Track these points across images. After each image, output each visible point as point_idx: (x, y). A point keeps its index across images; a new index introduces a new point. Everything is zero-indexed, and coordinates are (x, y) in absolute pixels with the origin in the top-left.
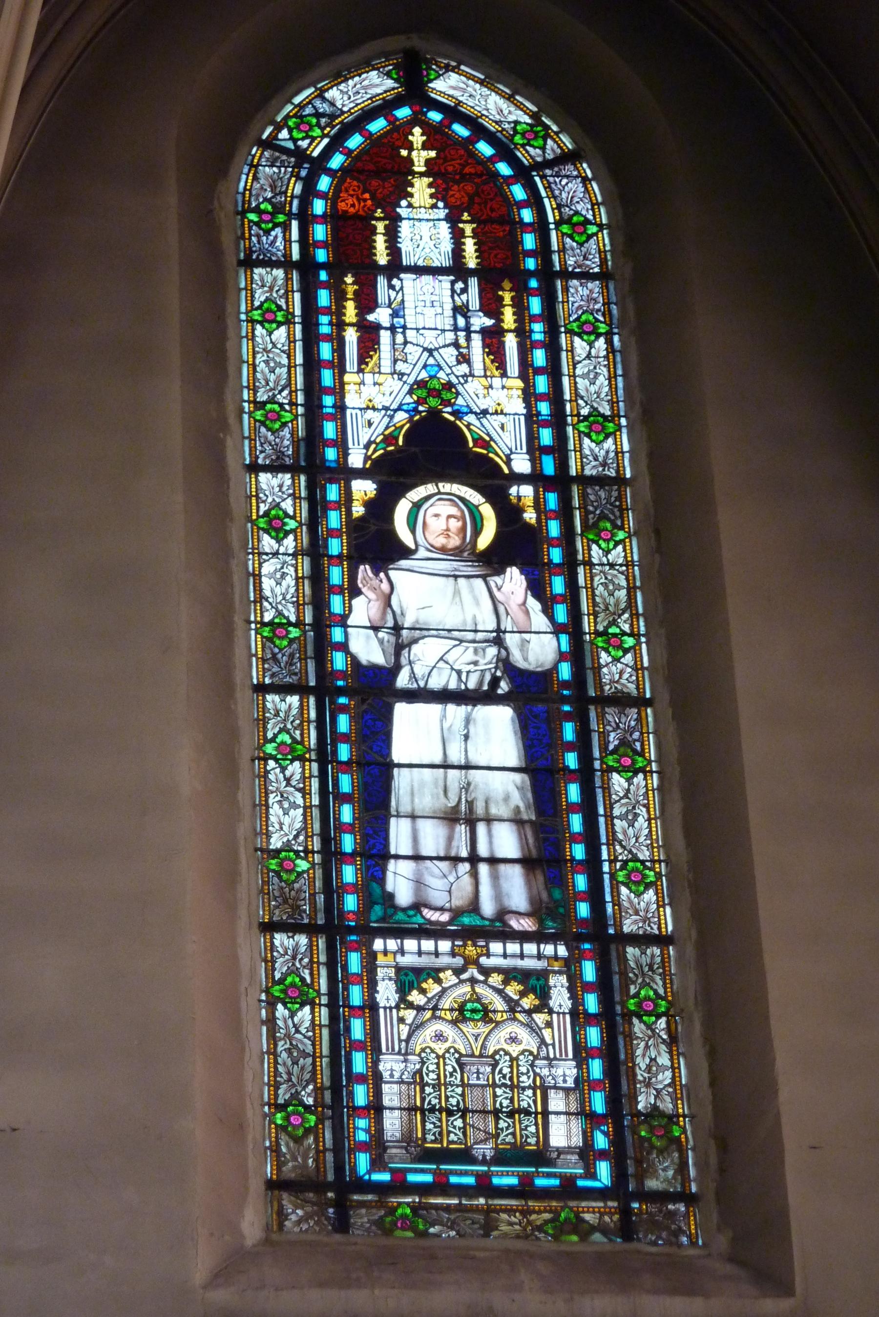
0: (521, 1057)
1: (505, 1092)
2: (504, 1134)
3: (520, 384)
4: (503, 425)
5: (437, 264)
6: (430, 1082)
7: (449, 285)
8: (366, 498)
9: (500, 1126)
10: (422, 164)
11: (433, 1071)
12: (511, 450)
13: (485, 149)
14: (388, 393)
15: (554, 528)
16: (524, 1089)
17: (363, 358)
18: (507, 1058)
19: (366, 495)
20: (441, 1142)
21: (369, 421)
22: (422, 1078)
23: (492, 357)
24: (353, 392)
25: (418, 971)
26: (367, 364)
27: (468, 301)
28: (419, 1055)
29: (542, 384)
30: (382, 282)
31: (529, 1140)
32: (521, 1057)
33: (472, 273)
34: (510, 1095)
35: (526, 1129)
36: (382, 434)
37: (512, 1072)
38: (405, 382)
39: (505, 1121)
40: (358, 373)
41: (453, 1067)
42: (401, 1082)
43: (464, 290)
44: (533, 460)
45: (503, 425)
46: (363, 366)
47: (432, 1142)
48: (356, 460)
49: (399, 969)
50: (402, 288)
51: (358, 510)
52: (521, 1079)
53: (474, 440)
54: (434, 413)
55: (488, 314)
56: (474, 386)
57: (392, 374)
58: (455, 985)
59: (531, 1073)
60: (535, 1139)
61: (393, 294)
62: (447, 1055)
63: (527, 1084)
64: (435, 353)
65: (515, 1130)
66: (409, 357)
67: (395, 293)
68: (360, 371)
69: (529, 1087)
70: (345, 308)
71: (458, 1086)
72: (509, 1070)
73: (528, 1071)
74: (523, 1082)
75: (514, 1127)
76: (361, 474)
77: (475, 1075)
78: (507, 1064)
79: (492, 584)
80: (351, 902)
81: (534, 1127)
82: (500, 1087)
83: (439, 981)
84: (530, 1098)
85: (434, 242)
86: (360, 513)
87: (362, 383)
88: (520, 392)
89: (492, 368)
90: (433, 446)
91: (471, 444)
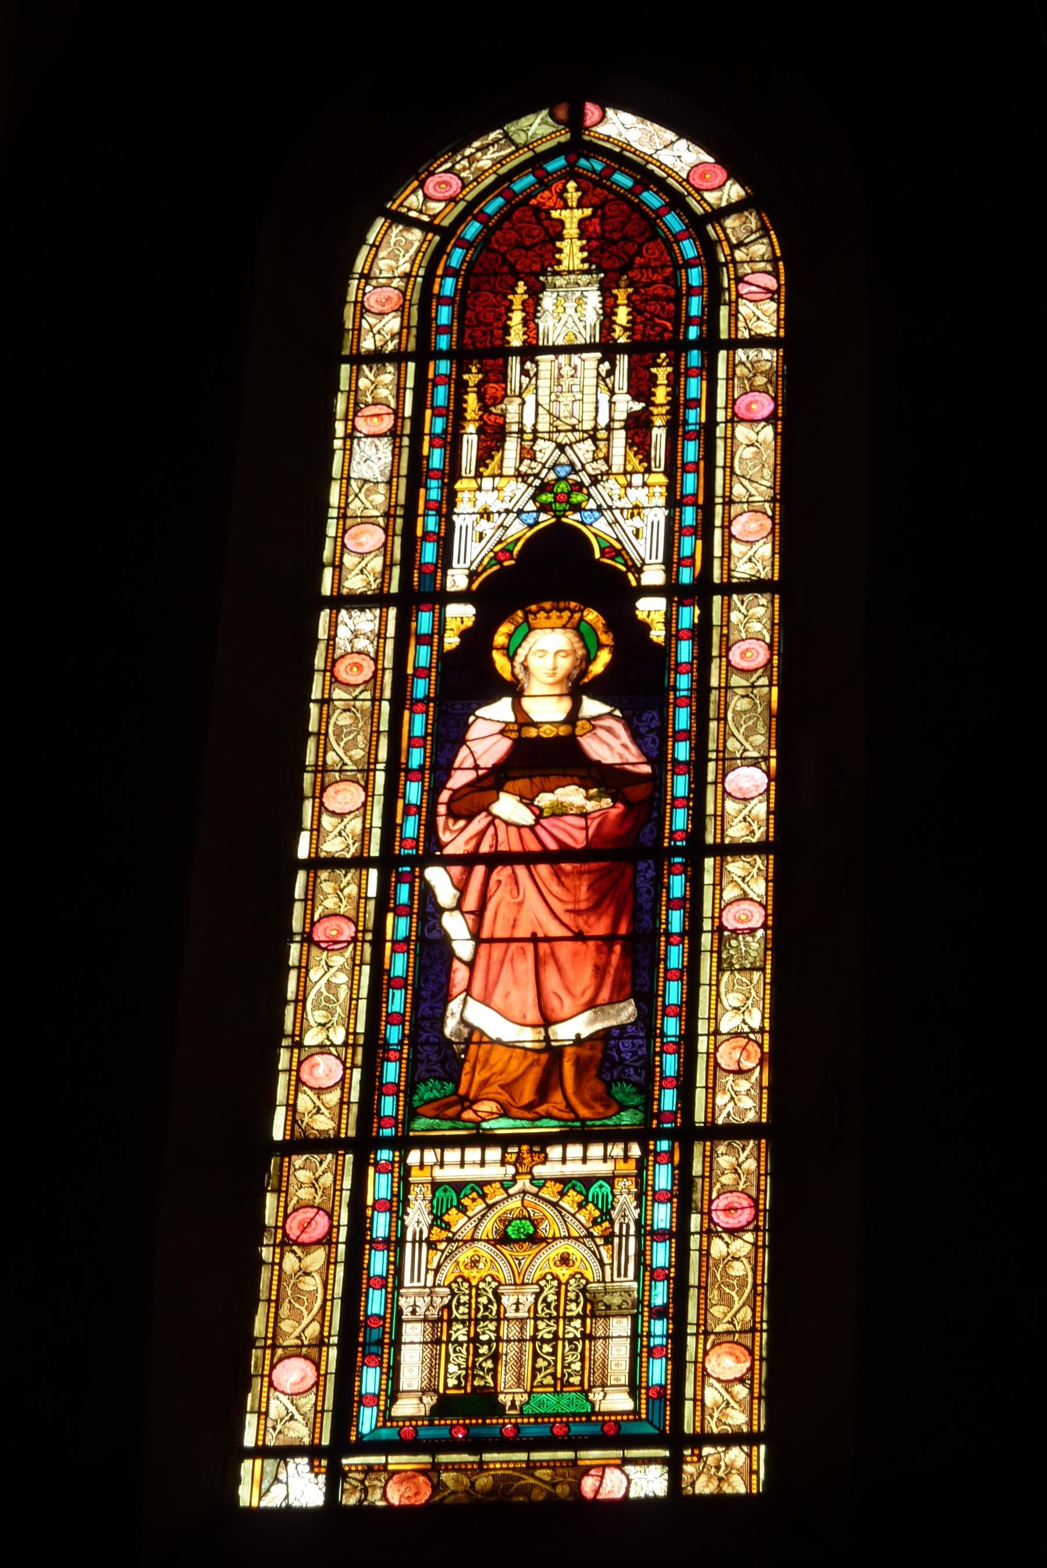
0: (572, 1281)
1: (548, 1325)
2: (543, 1374)
3: (663, 479)
4: (638, 530)
5: (581, 341)
6: (459, 1317)
7: (594, 364)
8: (462, 627)
9: (537, 1366)
10: (575, 225)
11: (464, 1304)
12: (643, 560)
13: (652, 199)
14: (507, 499)
15: (685, 651)
16: (571, 1319)
17: (484, 458)
18: (555, 1283)
19: (462, 622)
20: (465, 1388)
21: (481, 534)
22: (450, 1313)
23: (635, 449)
24: (466, 500)
25: (458, 1186)
26: (486, 466)
27: (613, 385)
28: (449, 1286)
29: (690, 483)
30: (515, 363)
31: (572, 1380)
32: (572, 1281)
33: (622, 349)
34: (554, 1329)
35: (569, 1367)
36: (492, 550)
37: (558, 1300)
38: (530, 485)
39: (544, 1359)
40: (475, 478)
41: (489, 1299)
42: (425, 1320)
43: (611, 373)
44: (668, 571)
45: (638, 530)
46: (481, 469)
47: (455, 1387)
48: (457, 580)
49: (435, 1185)
50: (536, 374)
51: (452, 641)
52: (568, 1308)
53: (602, 550)
54: (559, 529)
55: (636, 398)
56: (611, 487)
57: (516, 477)
58: (503, 1200)
59: (581, 1299)
60: (579, 1378)
61: (525, 380)
62: (482, 1285)
63: (574, 1314)
64: (567, 449)
65: (556, 1369)
66: (538, 455)
67: (527, 379)
68: (479, 475)
69: (578, 1316)
70: (466, 401)
71: (491, 1320)
72: (555, 1297)
73: (578, 1296)
74: (571, 1310)
75: (555, 1366)
76: (460, 597)
77: (514, 1307)
78: (553, 1291)
79: (613, 1382)
80: (388, 1106)
81: (579, 1364)
82: (542, 1319)
83: (483, 1196)
84: (577, 1329)
85: (579, 314)
86: (454, 646)
87: (480, 489)
88: (664, 489)
89: (634, 462)
90: (556, 568)
91: (597, 555)
